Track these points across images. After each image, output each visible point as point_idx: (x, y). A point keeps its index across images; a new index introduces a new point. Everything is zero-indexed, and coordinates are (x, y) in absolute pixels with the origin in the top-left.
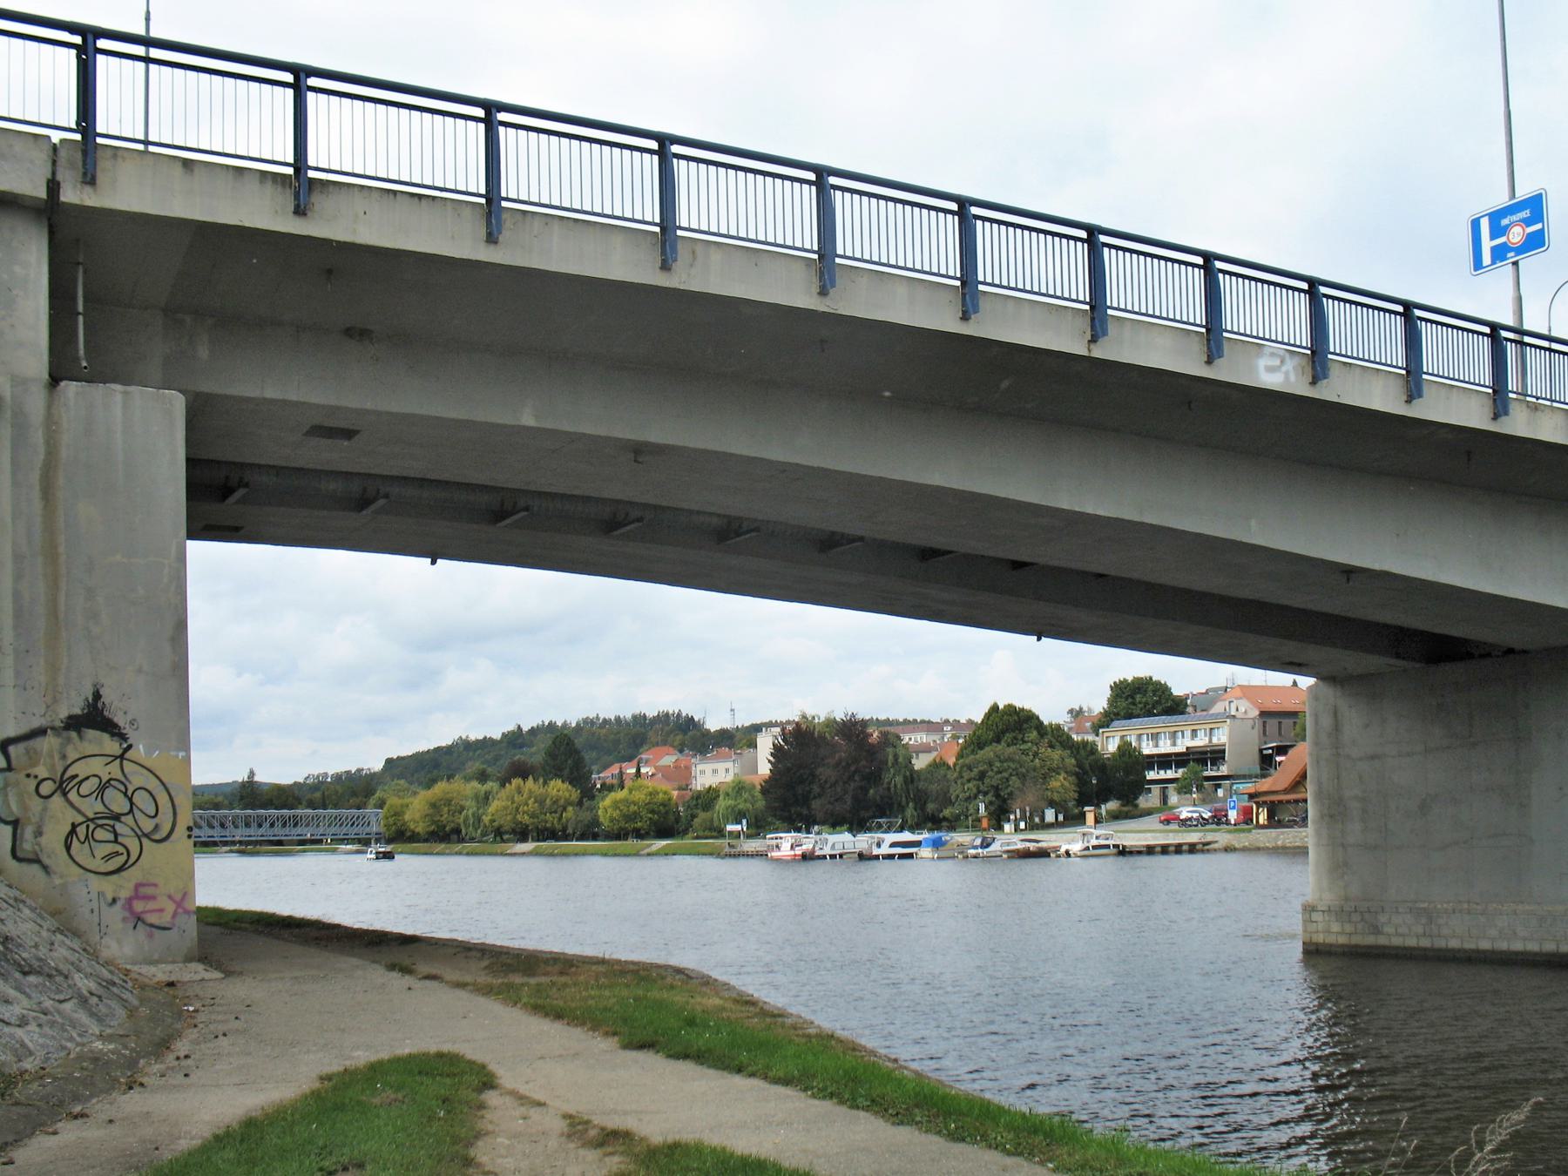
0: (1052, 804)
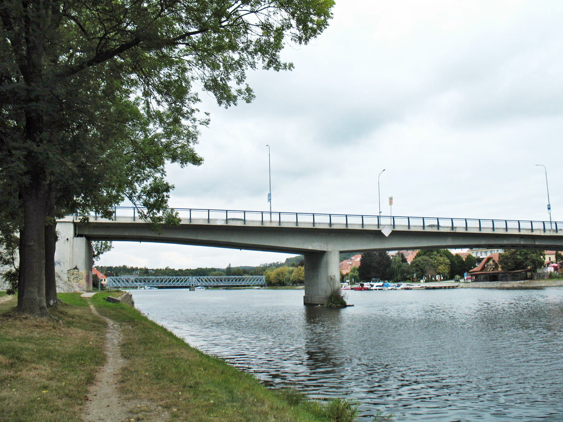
0: (439, 274)
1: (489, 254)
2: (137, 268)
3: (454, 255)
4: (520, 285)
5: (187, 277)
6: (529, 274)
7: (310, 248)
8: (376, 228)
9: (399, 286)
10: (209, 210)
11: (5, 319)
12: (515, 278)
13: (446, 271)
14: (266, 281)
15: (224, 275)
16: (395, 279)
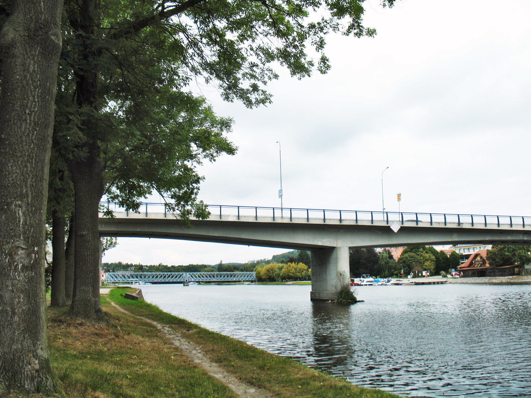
0: (425, 270)
1: (477, 251)
2: (132, 264)
3: (439, 252)
4: (509, 281)
5: (181, 273)
6: (516, 270)
7: (320, 244)
8: (385, 224)
9: (389, 281)
10: (221, 206)
11: (56, 325)
12: (503, 273)
13: (432, 267)
14: (256, 277)
15: (215, 272)
16: (383, 275)
